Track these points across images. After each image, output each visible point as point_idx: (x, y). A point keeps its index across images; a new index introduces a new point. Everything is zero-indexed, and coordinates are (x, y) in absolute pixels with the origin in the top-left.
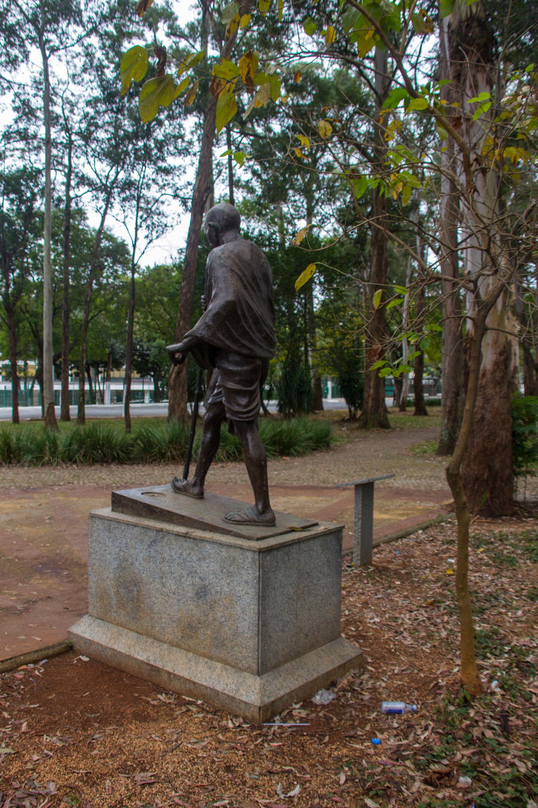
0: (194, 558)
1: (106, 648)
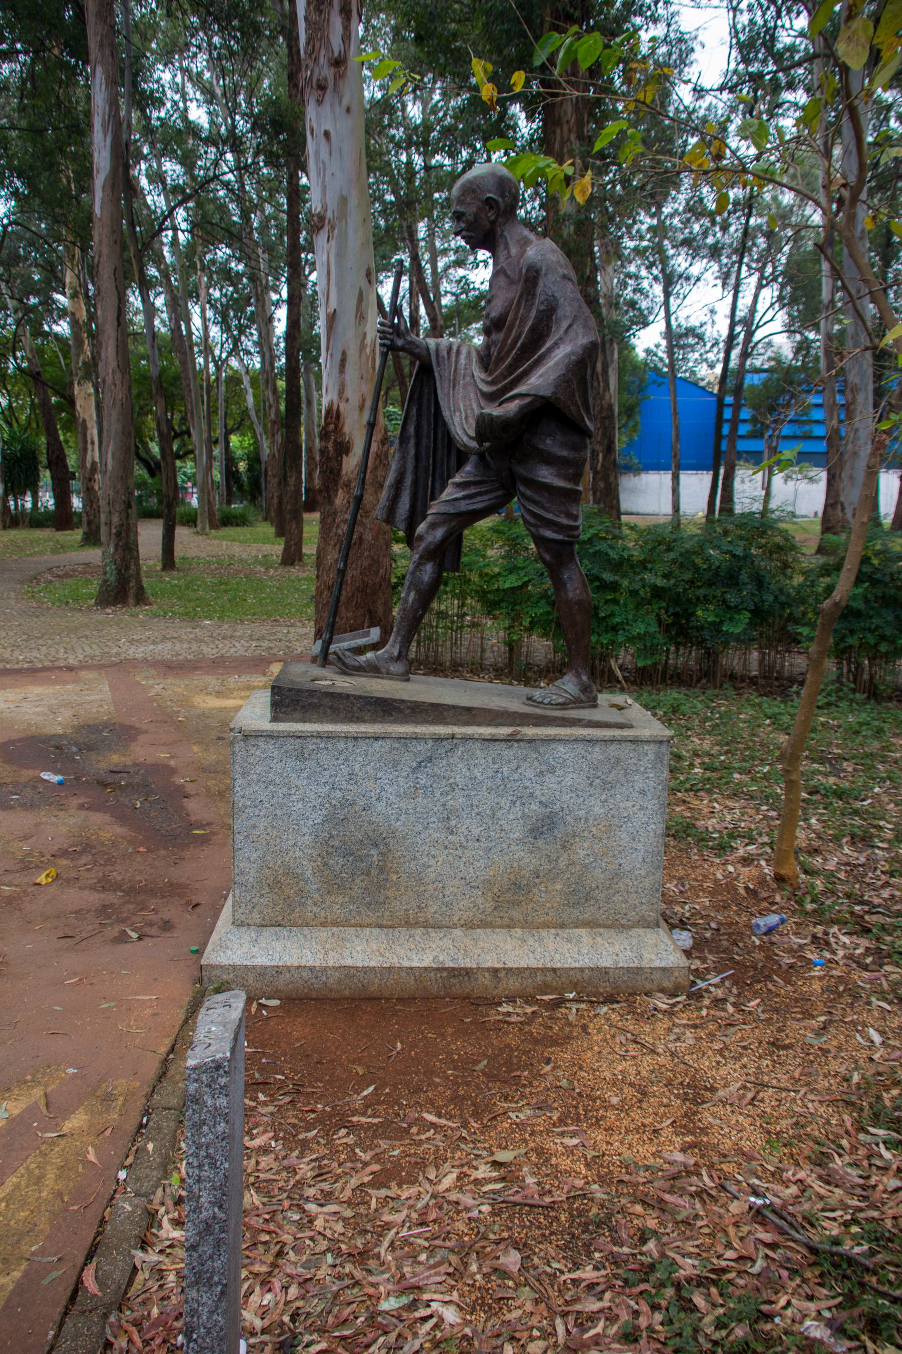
0: (530, 774)
1: (325, 969)
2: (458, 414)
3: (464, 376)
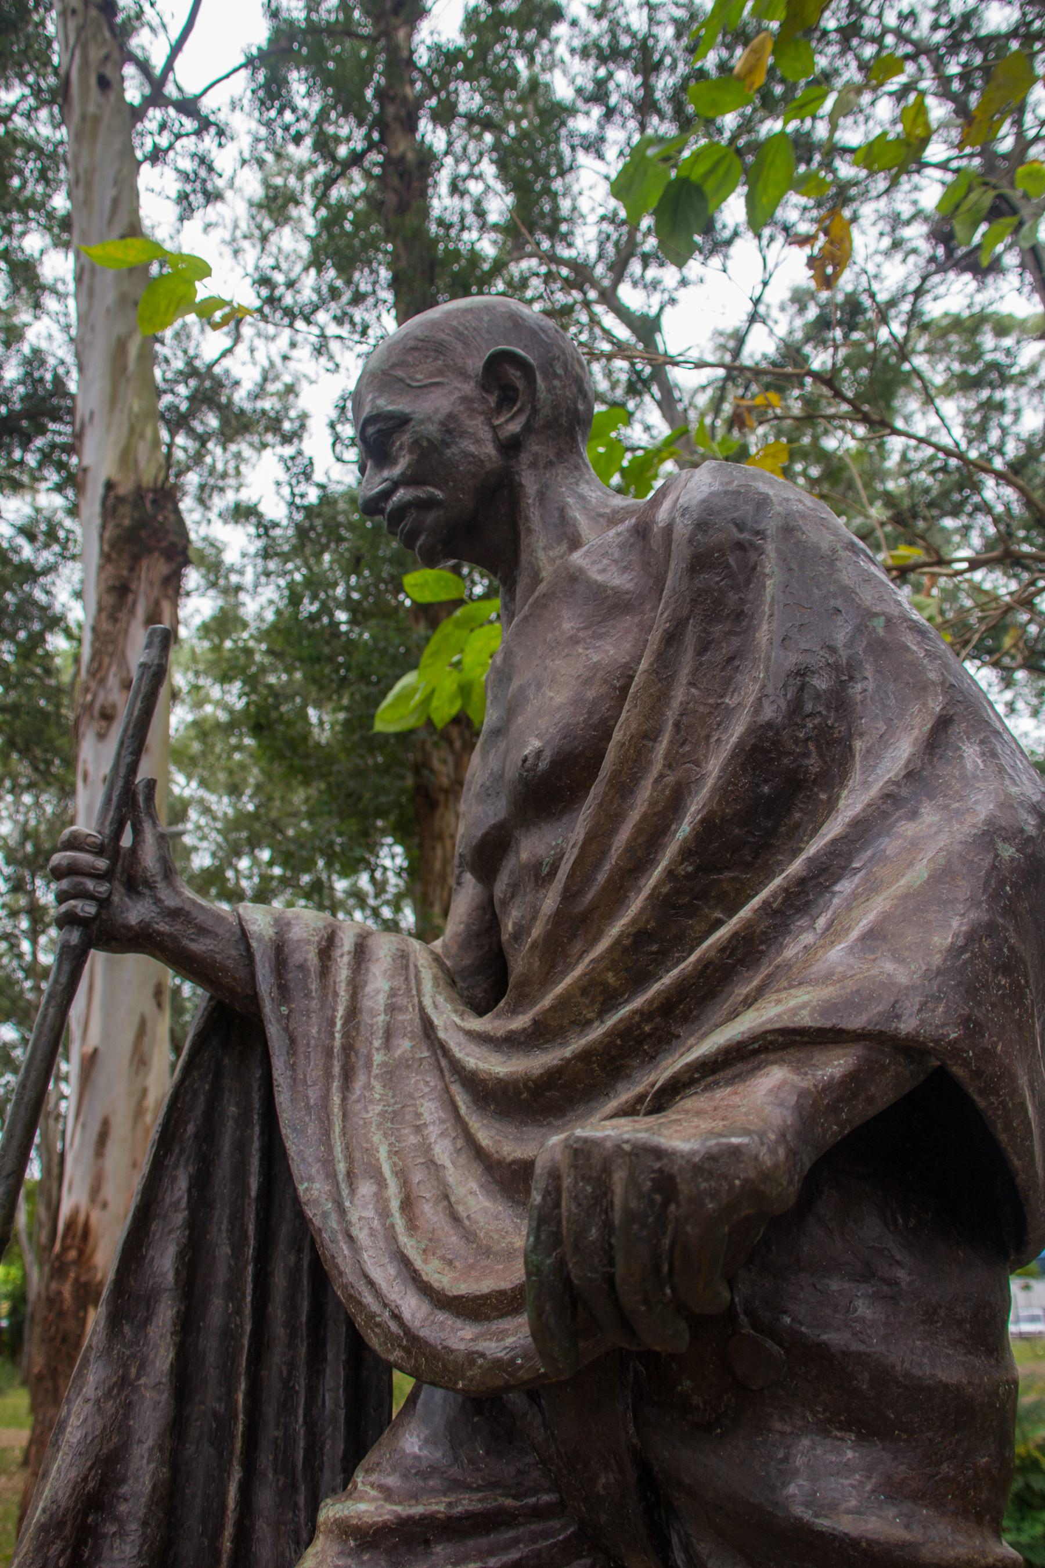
2: (366, 1188)
3: (388, 1035)
